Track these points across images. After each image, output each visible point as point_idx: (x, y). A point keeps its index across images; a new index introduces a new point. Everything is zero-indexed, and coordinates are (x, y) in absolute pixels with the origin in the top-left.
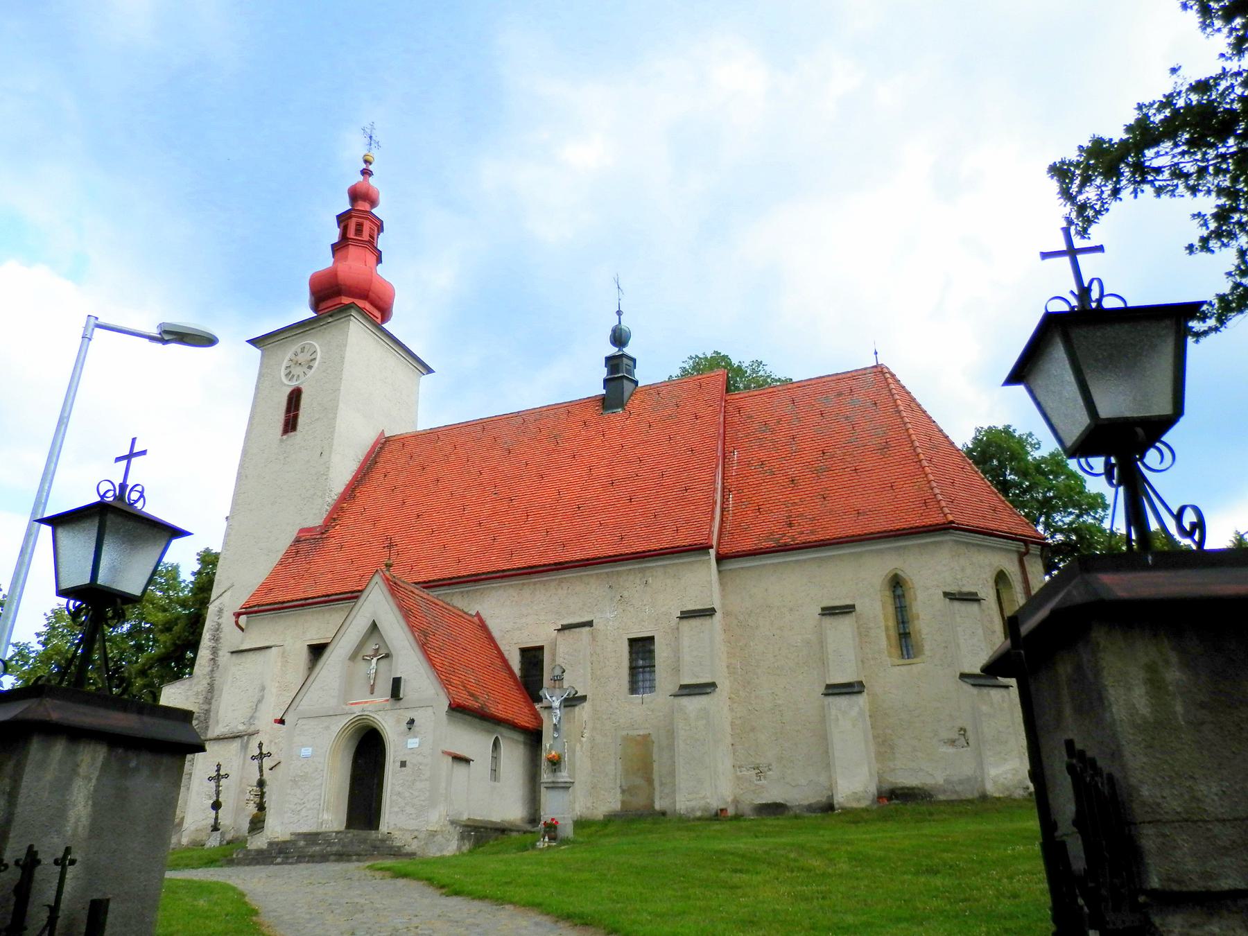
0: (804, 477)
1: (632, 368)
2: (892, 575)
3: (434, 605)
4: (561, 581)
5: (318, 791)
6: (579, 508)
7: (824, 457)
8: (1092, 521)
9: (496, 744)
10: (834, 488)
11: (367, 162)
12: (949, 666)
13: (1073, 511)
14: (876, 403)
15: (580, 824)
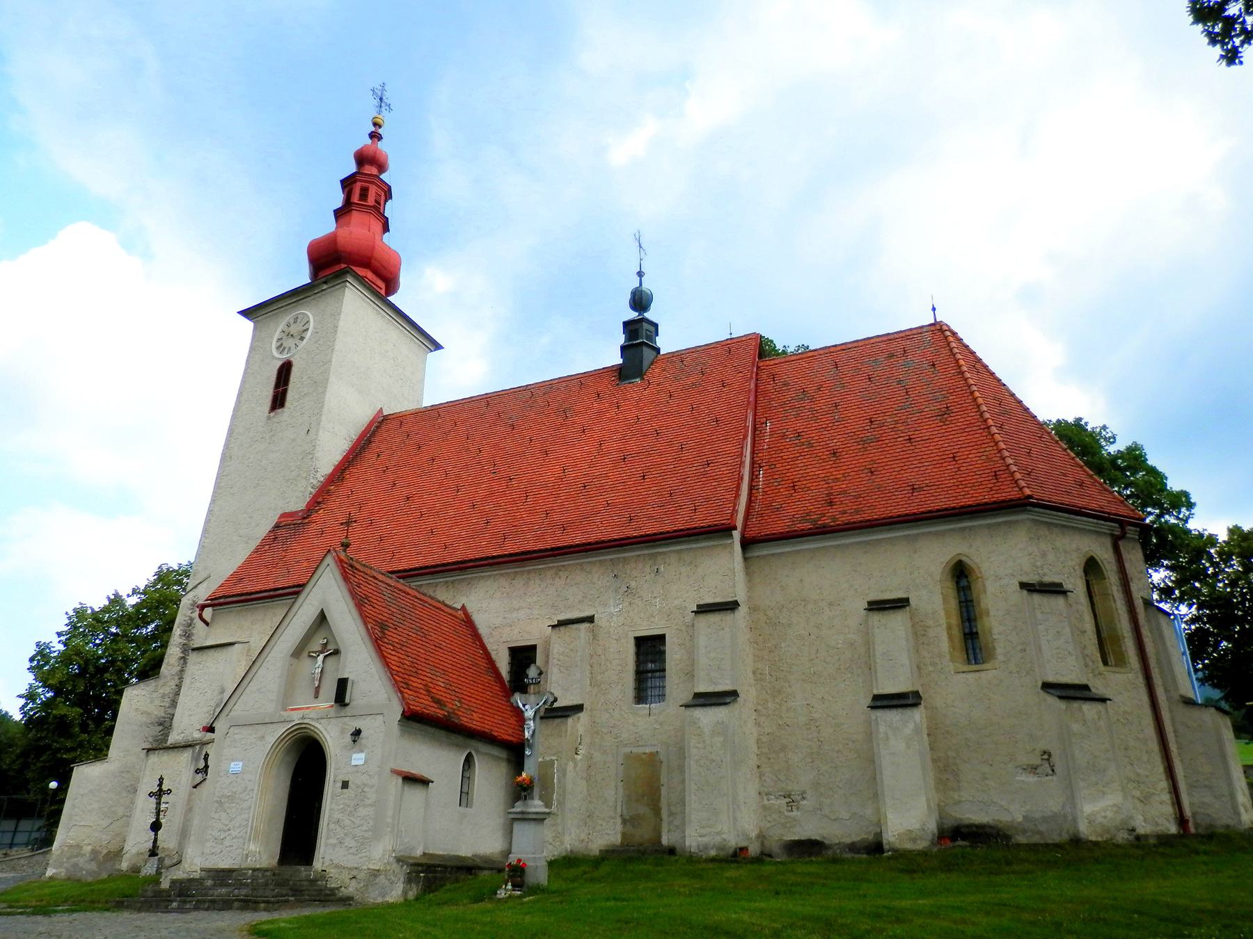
0: (848, 449)
1: (654, 334)
2: (955, 561)
3: (403, 594)
4: (559, 569)
5: (245, 816)
6: (585, 486)
7: (872, 426)
8: (1176, 522)
9: (469, 762)
10: (883, 460)
11: (375, 124)
12: (1028, 673)
13: (1153, 511)
14: (934, 365)
15: (565, 864)
